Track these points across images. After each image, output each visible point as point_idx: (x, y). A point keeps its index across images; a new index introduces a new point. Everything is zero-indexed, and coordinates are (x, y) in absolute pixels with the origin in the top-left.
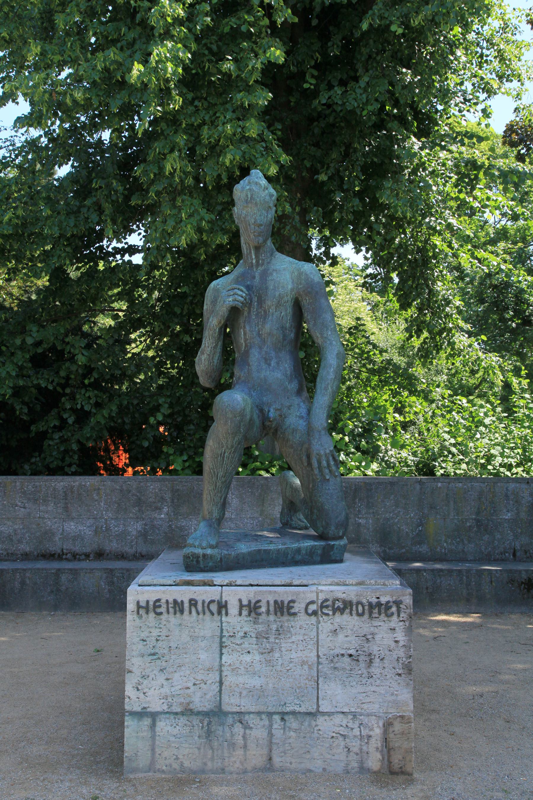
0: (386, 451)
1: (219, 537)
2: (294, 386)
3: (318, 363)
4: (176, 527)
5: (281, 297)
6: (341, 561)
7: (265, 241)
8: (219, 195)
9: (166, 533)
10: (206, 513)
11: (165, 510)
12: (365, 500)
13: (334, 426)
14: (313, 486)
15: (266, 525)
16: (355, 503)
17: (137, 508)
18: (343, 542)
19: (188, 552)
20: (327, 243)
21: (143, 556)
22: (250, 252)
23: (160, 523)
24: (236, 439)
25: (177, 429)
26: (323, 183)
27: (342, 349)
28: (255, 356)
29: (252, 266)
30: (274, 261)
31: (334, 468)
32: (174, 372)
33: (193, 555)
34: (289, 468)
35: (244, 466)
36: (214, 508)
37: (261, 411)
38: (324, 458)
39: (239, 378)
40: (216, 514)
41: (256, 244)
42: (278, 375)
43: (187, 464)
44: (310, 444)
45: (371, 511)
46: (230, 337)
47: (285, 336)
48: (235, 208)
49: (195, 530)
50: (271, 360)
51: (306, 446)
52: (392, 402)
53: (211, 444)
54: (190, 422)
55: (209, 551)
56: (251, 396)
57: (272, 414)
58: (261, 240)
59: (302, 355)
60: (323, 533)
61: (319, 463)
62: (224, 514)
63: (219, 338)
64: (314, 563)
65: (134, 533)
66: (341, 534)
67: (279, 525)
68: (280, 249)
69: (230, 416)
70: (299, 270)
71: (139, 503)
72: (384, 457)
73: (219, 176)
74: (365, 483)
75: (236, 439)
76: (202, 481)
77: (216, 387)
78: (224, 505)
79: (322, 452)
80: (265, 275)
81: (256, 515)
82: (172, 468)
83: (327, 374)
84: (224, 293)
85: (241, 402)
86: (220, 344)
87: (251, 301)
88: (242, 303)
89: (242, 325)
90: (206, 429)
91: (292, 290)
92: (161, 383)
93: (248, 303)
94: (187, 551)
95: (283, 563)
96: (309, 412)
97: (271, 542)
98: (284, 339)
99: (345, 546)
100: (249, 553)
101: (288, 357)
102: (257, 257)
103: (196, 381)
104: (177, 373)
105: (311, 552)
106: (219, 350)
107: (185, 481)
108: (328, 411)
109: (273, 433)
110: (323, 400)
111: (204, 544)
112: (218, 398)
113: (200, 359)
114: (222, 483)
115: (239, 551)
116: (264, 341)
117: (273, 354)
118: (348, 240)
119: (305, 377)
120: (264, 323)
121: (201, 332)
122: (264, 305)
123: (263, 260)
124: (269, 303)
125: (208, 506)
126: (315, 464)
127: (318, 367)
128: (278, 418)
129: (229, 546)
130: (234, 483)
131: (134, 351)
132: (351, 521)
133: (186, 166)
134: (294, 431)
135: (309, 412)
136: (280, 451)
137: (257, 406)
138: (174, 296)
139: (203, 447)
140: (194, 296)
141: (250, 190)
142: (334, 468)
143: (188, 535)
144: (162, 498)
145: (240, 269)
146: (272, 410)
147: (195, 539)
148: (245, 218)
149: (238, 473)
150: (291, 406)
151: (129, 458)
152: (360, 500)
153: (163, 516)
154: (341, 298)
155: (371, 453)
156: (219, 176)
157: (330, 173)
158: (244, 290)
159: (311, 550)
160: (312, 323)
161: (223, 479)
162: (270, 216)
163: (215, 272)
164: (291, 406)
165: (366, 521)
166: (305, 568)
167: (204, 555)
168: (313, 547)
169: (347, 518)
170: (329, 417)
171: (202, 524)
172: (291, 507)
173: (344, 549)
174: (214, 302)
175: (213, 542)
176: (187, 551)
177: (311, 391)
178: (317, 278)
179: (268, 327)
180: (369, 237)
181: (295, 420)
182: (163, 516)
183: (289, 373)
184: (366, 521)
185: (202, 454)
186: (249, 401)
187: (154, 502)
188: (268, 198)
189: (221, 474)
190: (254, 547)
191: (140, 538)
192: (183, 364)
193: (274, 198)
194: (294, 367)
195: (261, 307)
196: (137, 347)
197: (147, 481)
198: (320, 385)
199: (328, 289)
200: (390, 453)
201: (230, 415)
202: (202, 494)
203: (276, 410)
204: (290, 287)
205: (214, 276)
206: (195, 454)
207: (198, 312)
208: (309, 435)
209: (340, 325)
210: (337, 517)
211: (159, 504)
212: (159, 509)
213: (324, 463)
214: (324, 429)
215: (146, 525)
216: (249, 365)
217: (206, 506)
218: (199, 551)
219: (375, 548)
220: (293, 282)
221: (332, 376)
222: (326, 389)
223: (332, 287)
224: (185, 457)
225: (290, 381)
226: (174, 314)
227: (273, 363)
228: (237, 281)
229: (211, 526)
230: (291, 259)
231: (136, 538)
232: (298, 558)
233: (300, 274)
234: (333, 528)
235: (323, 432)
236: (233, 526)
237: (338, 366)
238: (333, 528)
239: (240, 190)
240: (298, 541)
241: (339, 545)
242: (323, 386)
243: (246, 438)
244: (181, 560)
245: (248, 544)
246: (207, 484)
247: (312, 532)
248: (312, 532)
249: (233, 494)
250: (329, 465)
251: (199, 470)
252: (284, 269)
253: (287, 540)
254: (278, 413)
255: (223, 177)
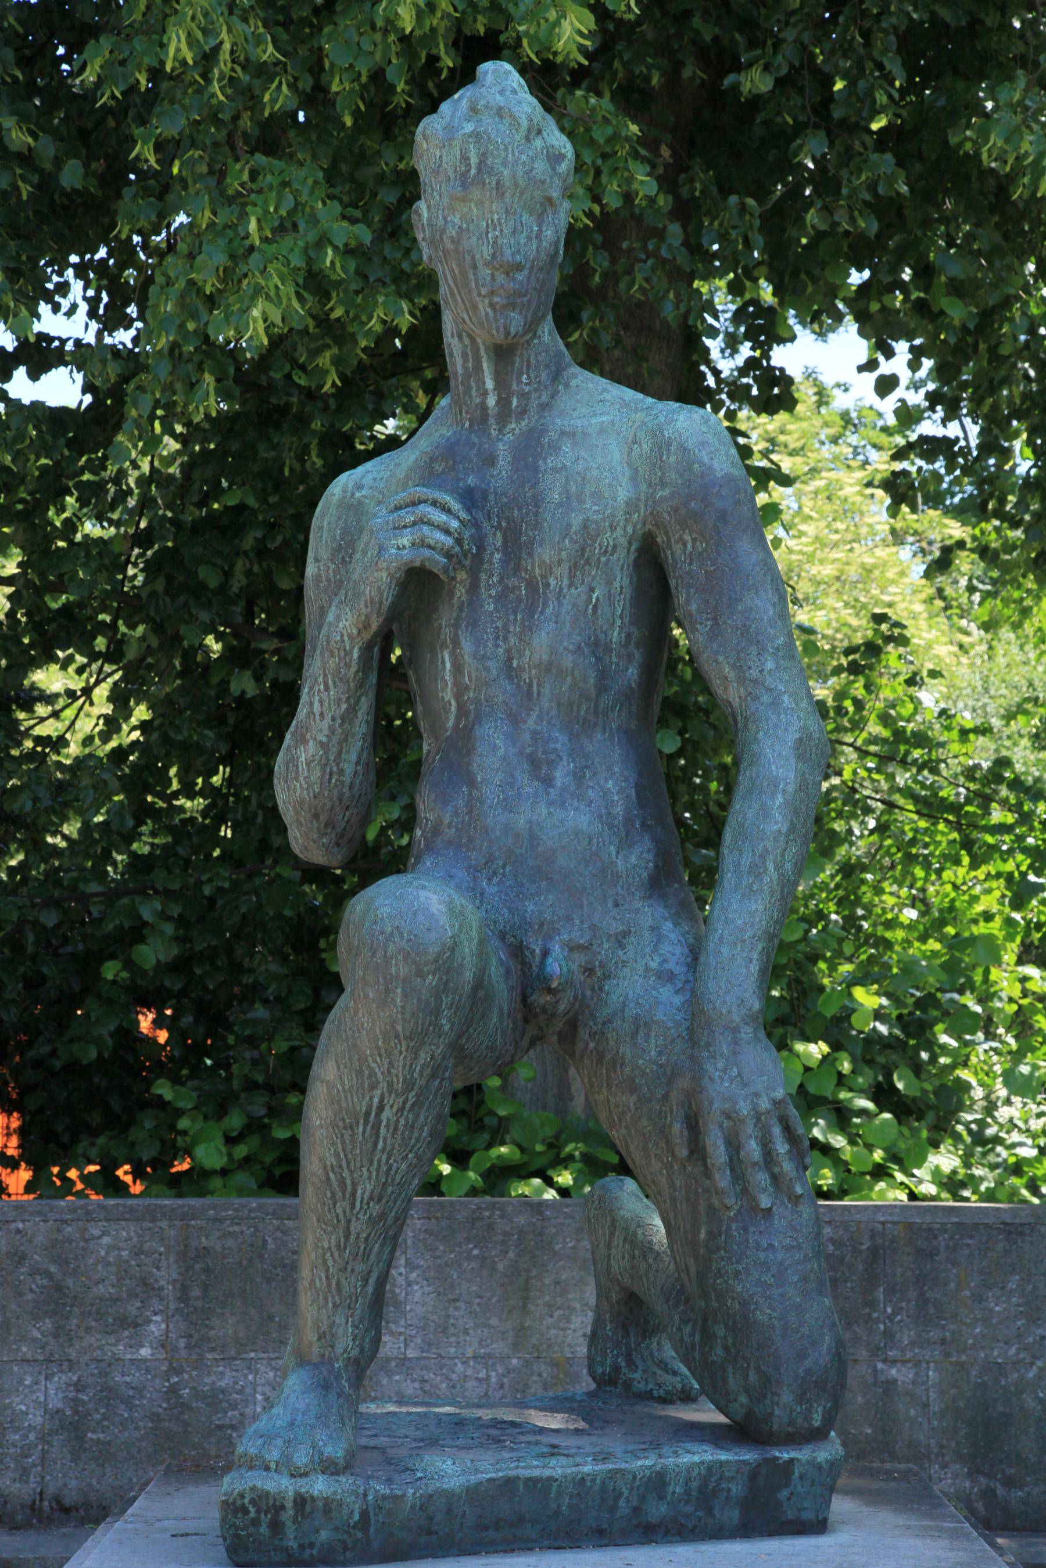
0: (991, 1108)
1: (359, 1429)
2: (637, 859)
3: (728, 777)
4: (197, 1394)
5: (589, 531)
6: (819, 1526)
7: (532, 327)
8: (367, 155)
9: (155, 1418)
10: (310, 1335)
11: (156, 1327)
12: (912, 1294)
13: (794, 1008)
14: (712, 1236)
15: (536, 1388)
16: (872, 1304)
17: (48, 1324)
18: (828, 1451)
19: (239, 1487)
20: (764, 329)
21: (65, 1510)
22: (478, 367)
23: (135, 1377)
24: (424, 1056)
25: (207, 1017)
26: (756, 101)
27: (813, 723)
28: (494, 750)
29: (484, 419)
30: (563, 402)
31: (788, 1167)
32: (192, 805)
33: (260, 1498)
34: (624, 1169)
35: (459, 1158)
36: (339, 1319)
37: (518, 951)
38: (749, 1128)
39: (436, 831)
40: (345, 1342)
41: (500, 338)
42: (580, 819)
43: (241, 1151)
44: (698, 1075)
45: (934, 1335)
46: (404, 678)
47: (603, 674)
48: (422, 205)
49: (269, 1404)
50: (552, 764)
51: (684, 1083)
52: (1009, 922)
53: (329, 1076)
54: (254, 993)
55: (319, 1486)
56: (479, 896)
57: (556, 966)
58: (516, 321)
59: (669, 743)
60: (750, 1414)
61: (734, 1145)
62: (377, 1342)
63: (361, 685)
64: (718, 1533)
65: (36, 1419)
66: (817, 1420)
67: (586, 1384)
68: (592, 359)
69: (403, 971)
70: (656, 433)
71: (57, 1301)
72: (982, 1124)
73: (378, 76)
74: (909, 1226)
75: (424, 1056)
76: (295, 1215)
77: (350, 865)
78: (377, 1307)
79: (744, 1108)
80: (531, 451)
81: (499, 1347)
82: (182, 1166)
83: (764, 816)
84: (380, 518)
85: (444, 920)
86: (366, 704)
87: (481, 548)
88: (448, 555)
89: (447, 634)
90: (312, 1021)
91: (631, 506)
92: (141, 848)
93: (469, 557)
94: (236, 1483)
95: (601, 1532)
96: (695, 954)
97: (554, 1451)
98: (602, 689)
99: (833, 1468)
100: (472, 1492)
101: (616, 753)
102: (501, 384)
103: (276, 842)
104: (205, 813)
105: (706, 1489)
106: (361, 726)
107: (234, 1217)
108: (766, 953)
109: (562, 1037)
110: (742, 915)
111: (301, 1458)
112: (357, 906)
113: (293, 761)
114: (372, 1221)
115: (433, 1486)
116: (528, 697)
117: (560, 741)
118: (839, 318)
119: (680, 822)
120: (528, 629)
121: (297, 664)
122: (527, 564)
123: (524, 396)
124: (545, 553)
125: (317, 1311)
126: (718, 1152)
127: (729, 790)
128: (579, 977)
129: (395, 1466)
130: (416, 1223)
131: (40, 731)
132: (857, 1374)
133: (259, 41)
134: (640, 1025)
135: (695, 954)
136: (588, 1105)
137: (502, 936)
138: (197, 528)
139: (300, 1087)
140: (272, 527)
141: (476, 135)
142: (788, 1167)
143: (238, 1426)
144: (144, 1282)
145: (437, 431)
146: (556, 949)
147: (268, 1438)
148: (456, 242)
149: (434, 1186)
150: (625, 934)
151: (22, 1132)
152: (891, 1291)
153: (145, 1352)
154: (809, 528)
155: (932, 1111)
156: (378, 76)
157: (782, 65)
158: (456, 506)
159: (705, 1480)
160: (704, 628)
161: (376, 1209)
162: (549, 233)
163: (348, 441)
164: (625, 934)
165: (915, 1375)
166: (684, 1552)
167: (301, 1501)
168: (711, 1468)
169: (840, 1360)
170: (772, 973)
171: (294, 1382)
172: (628, 1315)
173: (827, 1478)
174: (345, 550)
175: (336, 1451)
176: (236, 1483)
177: (706, 878)
178: (723, 463)
179: (541, 643)
180: (921, 308)
181: (641, 983)
182: (145, 1352)
183: (619, 810)
184: (915, 1375)
185: (297, 1114)
186: (473, 916)
187: (115, 1300)
188: (541, 167)
189: (366, 1189)
190: (487, 1467)
191: (56, 1440)
192: (229, 781)
193: (563, 167)
194: (639, 788)
195: (517, 568)
196: (56, 715)
197: (89, 1217)
198: (735, 857)
199: (762, 499)
200: (1003, 1113)
201: (401, 969)
202: (294, 1267)
203: (573, 948)
204: (623, 494)
205: (344, 455)
206: (273, 1112)
207: (285, 584)
208: (692, 1039)
209: (809, 631)
210: (801, 1356)
211: (132, 1308)
212: (133, 1324)
213: (753, 1149)
214: (752, 1018)
215: (79, 1387)
216: (472, 783)
217: (311, 1310)
218: (282, 1485)
219: (949, 1479)
220: (633, 479)
221: (777, 822)
222: (757, 871)
223: (778, 492)
224: (235, 1121)
225: (626, 843)
226: (199, 591)
227: (560, 776)
228: (428, 473)
229: (326, 1387)
230: (629, 393)
231: (42, 1439)
232: (657, 1511)
233: (662, 446)
234: (787, 1397)
235: (747, 1033)
236: (410, 1389)
237: (803, 787)
238: (787, 1397)
239: (441, 138)
240: (656, 1446)
241: (812, 1463)
242: (747, 860)
243: (458, 1051)
244: (211, 1519)
245: (467, 1457)
246: (315, 1230)
247: (709, 1414)
248: (709, 1414)
249: (410, 1266)
250: (769, 1158)
251: (283, 1176)
252: (602, 431)
253: (614, 1442)
254: (580, 959)
255: (390, 74)
